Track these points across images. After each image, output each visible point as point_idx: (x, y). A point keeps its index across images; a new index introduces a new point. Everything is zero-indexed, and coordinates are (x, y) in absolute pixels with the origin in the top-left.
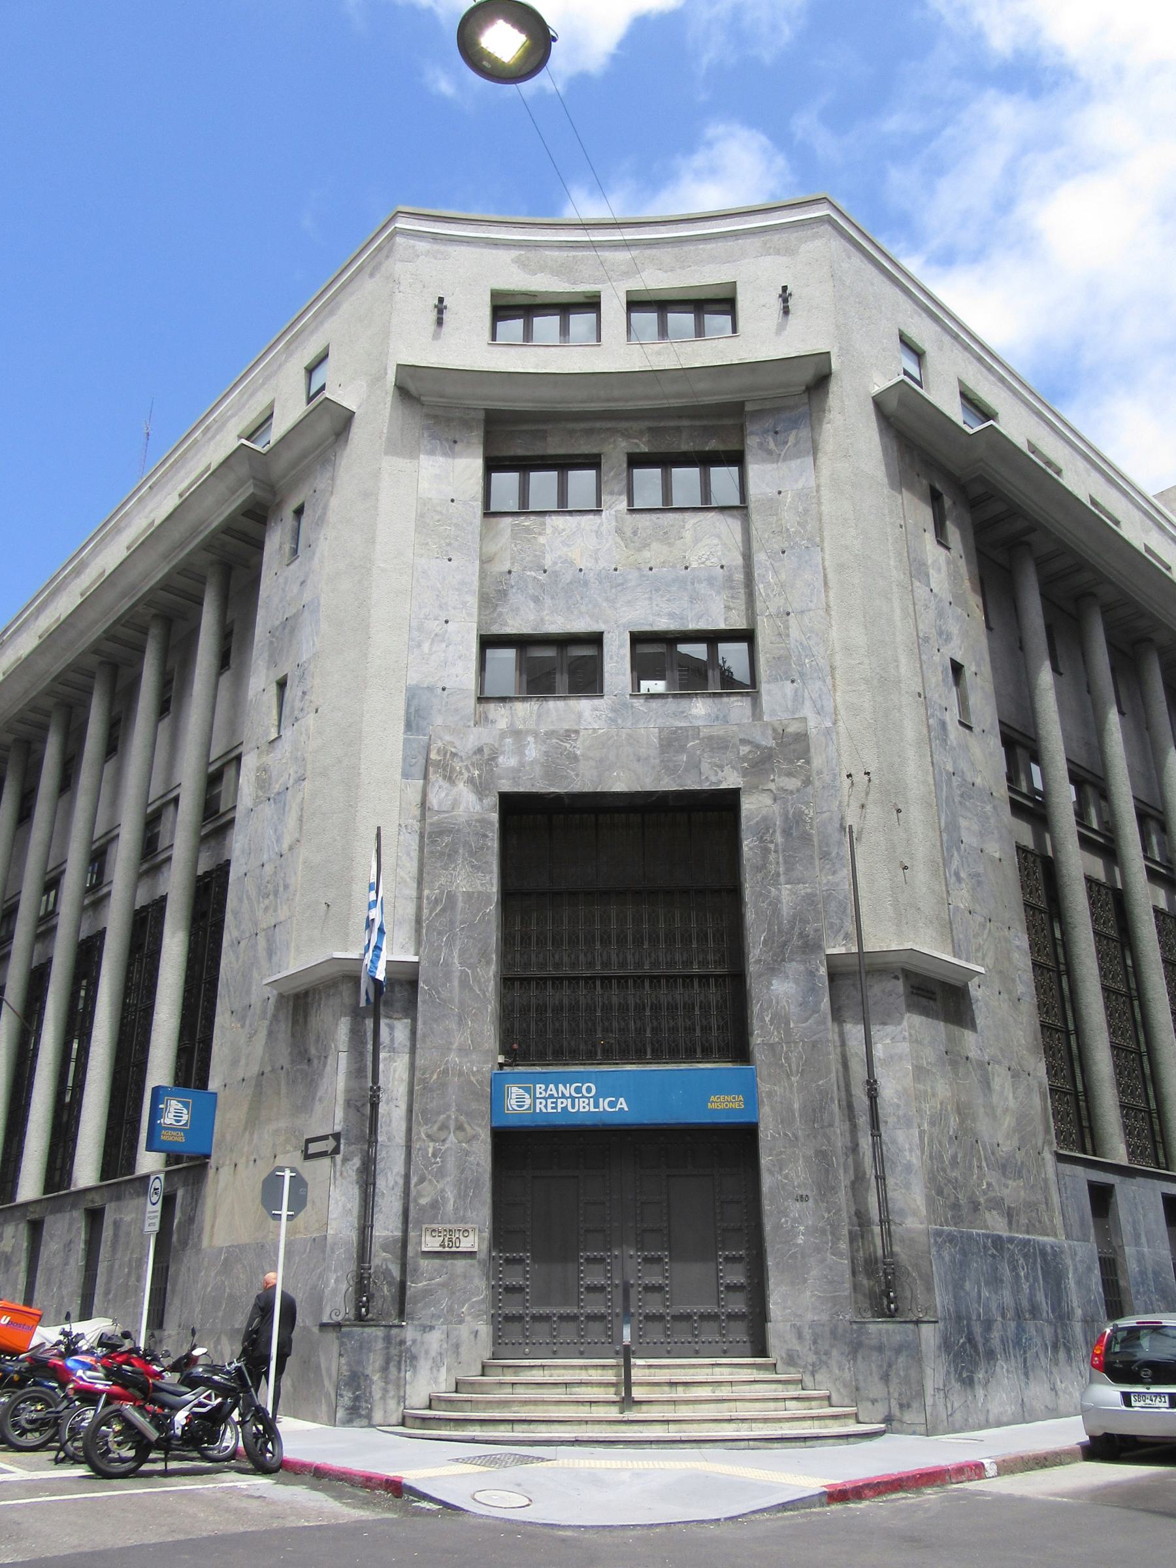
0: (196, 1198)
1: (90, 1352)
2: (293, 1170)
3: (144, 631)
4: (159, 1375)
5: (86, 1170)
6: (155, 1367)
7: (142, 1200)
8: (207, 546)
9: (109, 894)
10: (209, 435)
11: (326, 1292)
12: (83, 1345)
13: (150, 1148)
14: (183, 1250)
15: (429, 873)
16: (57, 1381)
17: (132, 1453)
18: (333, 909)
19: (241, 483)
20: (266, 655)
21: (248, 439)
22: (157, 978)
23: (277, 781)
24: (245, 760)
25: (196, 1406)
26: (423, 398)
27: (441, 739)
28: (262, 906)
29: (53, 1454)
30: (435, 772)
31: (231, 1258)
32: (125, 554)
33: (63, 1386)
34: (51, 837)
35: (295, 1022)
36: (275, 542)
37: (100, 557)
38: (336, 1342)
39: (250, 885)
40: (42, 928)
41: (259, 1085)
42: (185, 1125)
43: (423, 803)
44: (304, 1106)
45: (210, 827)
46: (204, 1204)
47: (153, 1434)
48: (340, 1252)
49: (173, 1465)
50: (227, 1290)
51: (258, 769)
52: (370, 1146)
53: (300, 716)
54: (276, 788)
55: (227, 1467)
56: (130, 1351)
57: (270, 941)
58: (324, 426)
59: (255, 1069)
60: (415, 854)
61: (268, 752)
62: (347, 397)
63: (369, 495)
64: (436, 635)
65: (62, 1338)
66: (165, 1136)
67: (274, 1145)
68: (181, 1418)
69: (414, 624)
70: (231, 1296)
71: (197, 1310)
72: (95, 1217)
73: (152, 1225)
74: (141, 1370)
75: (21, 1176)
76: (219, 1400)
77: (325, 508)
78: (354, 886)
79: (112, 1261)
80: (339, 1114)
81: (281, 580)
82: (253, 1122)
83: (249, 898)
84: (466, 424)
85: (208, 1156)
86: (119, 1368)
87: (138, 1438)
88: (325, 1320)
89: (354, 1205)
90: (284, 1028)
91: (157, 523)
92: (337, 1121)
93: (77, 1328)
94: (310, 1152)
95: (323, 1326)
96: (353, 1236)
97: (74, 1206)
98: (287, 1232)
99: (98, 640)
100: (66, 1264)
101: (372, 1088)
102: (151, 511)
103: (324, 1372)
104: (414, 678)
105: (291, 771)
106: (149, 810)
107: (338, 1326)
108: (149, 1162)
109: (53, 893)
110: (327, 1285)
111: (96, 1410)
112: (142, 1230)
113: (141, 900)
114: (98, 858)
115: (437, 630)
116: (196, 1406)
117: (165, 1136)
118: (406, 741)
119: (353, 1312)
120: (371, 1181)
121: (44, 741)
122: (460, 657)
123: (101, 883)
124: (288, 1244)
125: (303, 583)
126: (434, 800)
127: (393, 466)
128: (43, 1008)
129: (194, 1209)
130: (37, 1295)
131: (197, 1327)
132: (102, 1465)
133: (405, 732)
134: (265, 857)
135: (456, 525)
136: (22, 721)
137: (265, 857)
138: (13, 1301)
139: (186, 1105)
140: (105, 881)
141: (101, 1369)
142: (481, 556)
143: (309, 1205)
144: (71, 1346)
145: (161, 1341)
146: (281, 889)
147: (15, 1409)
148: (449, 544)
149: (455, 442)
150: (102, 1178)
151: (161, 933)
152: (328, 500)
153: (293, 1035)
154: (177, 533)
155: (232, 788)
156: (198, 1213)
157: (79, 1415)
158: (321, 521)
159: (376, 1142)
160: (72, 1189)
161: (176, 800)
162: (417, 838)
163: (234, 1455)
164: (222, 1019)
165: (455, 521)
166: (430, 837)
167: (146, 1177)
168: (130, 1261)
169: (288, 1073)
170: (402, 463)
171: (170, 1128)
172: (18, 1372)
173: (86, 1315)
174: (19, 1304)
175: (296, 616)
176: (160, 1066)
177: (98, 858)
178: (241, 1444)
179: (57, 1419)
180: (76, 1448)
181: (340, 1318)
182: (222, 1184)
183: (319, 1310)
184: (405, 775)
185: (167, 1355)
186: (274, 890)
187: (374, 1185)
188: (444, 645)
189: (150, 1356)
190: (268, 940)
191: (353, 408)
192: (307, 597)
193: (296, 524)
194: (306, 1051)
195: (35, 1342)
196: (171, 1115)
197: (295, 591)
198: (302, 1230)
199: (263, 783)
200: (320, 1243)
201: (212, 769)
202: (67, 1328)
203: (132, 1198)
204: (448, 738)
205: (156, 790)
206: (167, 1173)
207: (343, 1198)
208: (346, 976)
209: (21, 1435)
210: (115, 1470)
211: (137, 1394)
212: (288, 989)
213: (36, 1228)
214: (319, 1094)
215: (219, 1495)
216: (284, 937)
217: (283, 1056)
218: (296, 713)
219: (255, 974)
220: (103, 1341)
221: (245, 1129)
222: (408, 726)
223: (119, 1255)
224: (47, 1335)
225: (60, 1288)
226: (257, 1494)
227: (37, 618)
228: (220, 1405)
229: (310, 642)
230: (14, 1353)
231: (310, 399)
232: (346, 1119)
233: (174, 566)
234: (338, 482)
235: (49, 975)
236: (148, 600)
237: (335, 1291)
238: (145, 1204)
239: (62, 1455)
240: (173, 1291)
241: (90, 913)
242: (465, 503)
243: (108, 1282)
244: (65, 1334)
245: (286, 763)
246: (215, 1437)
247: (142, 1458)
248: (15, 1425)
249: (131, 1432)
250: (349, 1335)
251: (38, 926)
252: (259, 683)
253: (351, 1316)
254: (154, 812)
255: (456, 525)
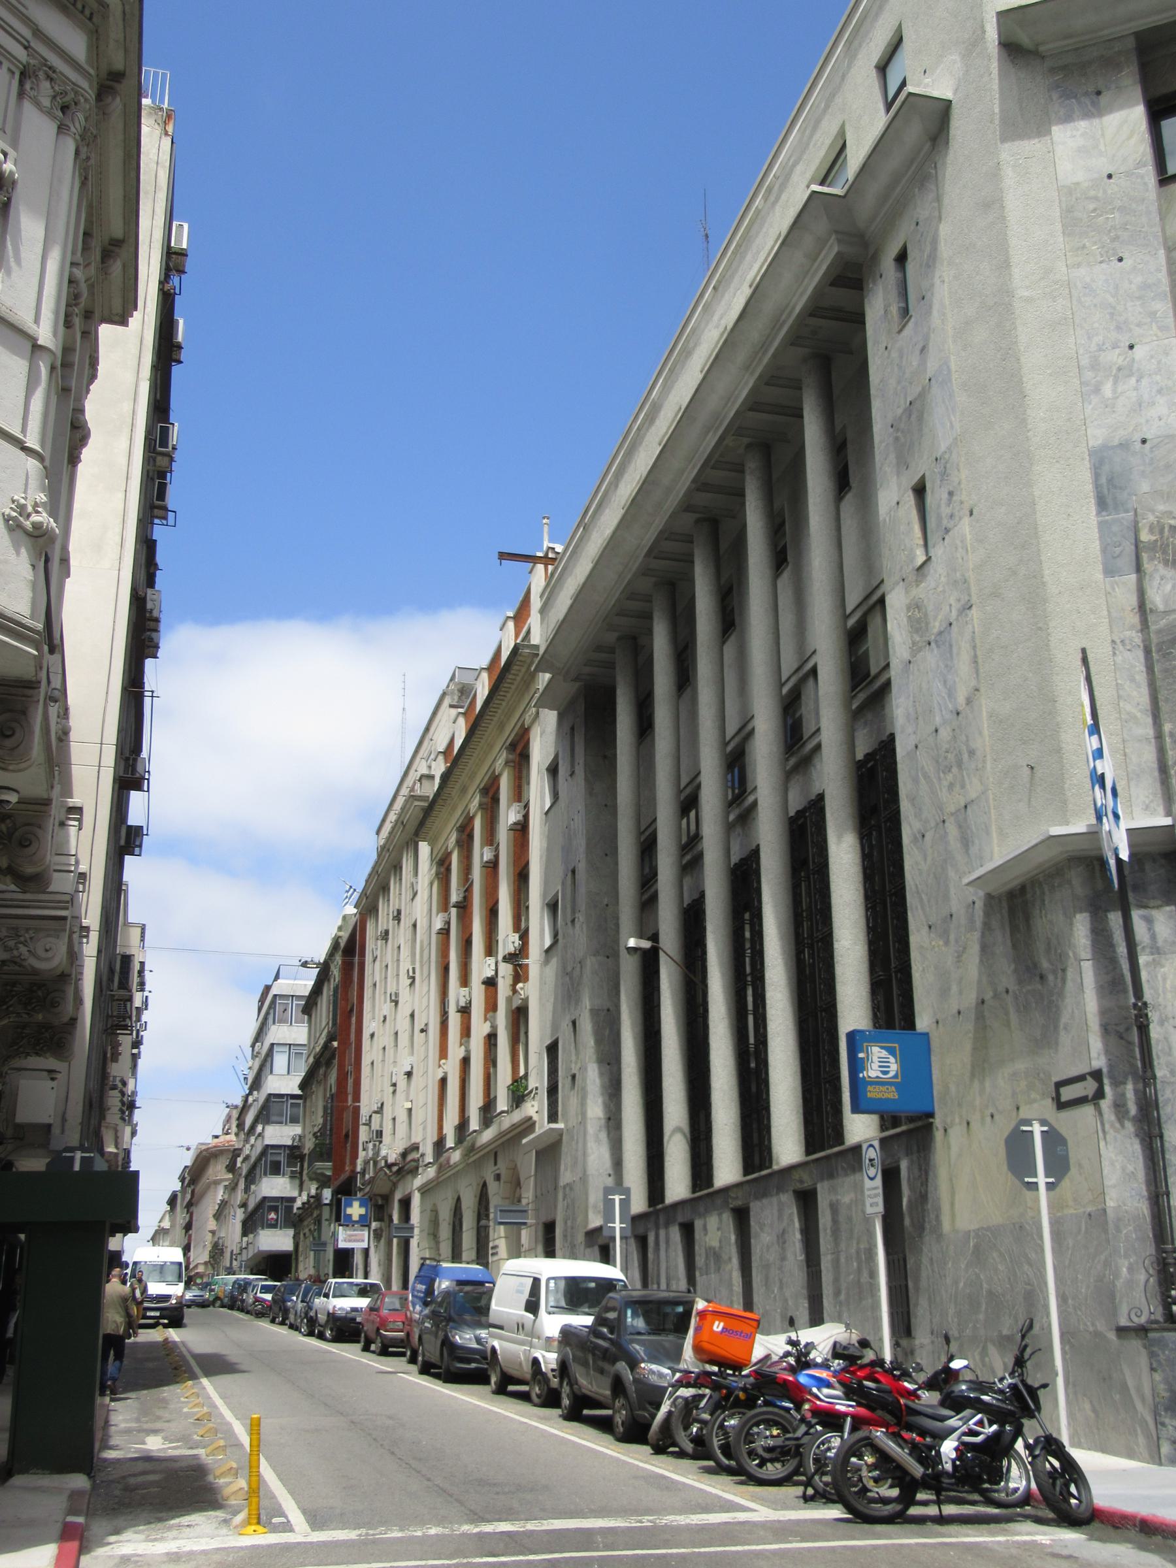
0: (924, 1169)
1: (825, 1365)
2: (1043, 1122)
3: (740, 469)
4: (913, 1394)
5: (787, 1145)
6: (906, 1384)
7: (857, 1176)
8: (795, 339)
9: (755, 803)
10: (772, 198)
11: (1119, 1284)
12: (817, 1356)
13: (856, 1109)
14: (920, 1236)
15: (1167, 700)
16: (792, 1402)
17: (895, 1492)
18: (1039, 772)
19: (822, 243)
20: (892, 457)
21: (822, 183)
22: (829, 897)
23: (935, 618)
24: (889, 600)
25: (965, 1434)
26: (1042, 49)
27: (1153, 511)
28: (945, 783)
29: (799, 1490)
30: (1152, 559)
31: (982, 1244)
32: (701, 376)
33: (798, 1408)
34: (678, 746)
35: (1014, 929)
36: (878, 306)
37: (673, 392)
38: (1144, 1352)
39: (925, 760)
40: (688, 857)
41: (980, 1017)
42: (896, 1076)
43: (1142, 607)
44: (1046, 1036)
45: (862, 697)
46: (936, 1176)
47: (917, 1470)
48: (1128, 1230)
49: (950, 1510)
50: (985, 1286)
51: (909, 608)
52: (1146, 1085)
53: (949, 526)
54: (936, 626)
55: (1019, 1515)
56: (873, 1364)
57: (963, 827)
58: (914, 132)
59: (971, 998)
60: (1142, 677)
61: (918, 583)
62: (937, 84)
63: (992, 204)
64: (1119, 369)
65: (789, 1348)
66: (873, 1093)
67: (1014, 1094)
68: (948, 1448)
69: (1085, 362)
70: (990, 1293)
71: (951, 1311)
72: (807, 1200)
73: (875, 1204)
74: (888, 1387)
75: (715, 1156)
76: (995, 1427)
77: (935, 242)
78: (1063, 736)
79: (836, 1253)
80: (1096, 1044)
81: (895, 355)
82: (981, 1065)
83: (926, 776)
84: (1110, 64)
85: (931, 1115)
86: (860, 1385)
87: (898, 1474)
88: (1123, 1322)
89: (1137, 1165)
90: (1001, 942)
91: (729, 328)
92: (1094, 1054)
93: (806, 1335)
94: (1064, 1099)
95: (1121, 1331)
96: (1143, 1207)
97: (780, 1189)
98: (1051, 1206)
99: (689, 493)
100: (783, 1258)
101: (1135, 1005)
102: (721, 318)
103: (1133, 1392)
104: (1097, 435)
105: (952, 601)
106: (785, 690)
107: (1142, 1331)
108: (860, 1128)
109: (693, 814)
110: (1117, 1275)
111: (842, 1437)
112: (863, 1212)
113: (796, 803)
114: (736, 761)
115: (1120, 361)
116: (965, 1434)
117: (873, 1093)
118: (1101, 525)
119: (1160, 1310)
120: (1157, 1131)
121: (650, 632)
122: (1159, 391)
123: (745, 791)
124: (1055, 1223)
125: (923, 349)
126: (1156, 598)
127: (1011, 153)
128: (704, 953)
129: (925, 1183)
130: (757, 1298)
131: (954, 1333)
132: (860, 1506)
133: (1098, 514)
134: (938, 719)
135: (1122, 209)
136: (621, 613)
137: (938, 719)
138: (731, 1306)
139: (891, 1051)
140: (749, 788)
141: (837, 1385)
142: (1165, 240)
143: (1073, 1170)
144: (803, 1361)
145: (912, 1352)
146: (966, 756)
147: (748, 1433)
148: (1117, 238)
149: (1099, 93)
150: (808, 1152)
151: (825, 841)
152: (937, 230)
153: (1014, 946)
154: (755, 333)
155: (881, 641)
156: (931, 1189)
157: (823, 1443)
158: (931, 262)
159: (1154, 1077)
160: (775, 1167)
161: (814, 671)
162: (1141, 654)
163: (1027, 1499)
164: (918, 938)
165: (1118, 203)
166: (1159, 651)
167: (857, 1149)
168: (858, 1252)
169: (1016, 998)
170: (1031, 146)
171: (877, 1082)
172: (744, 1389)
173: (816, 1319)
174: (738, 1309)
175: (922, 395)
176: (853, 1007)
177: (736, 761)
178: (1033, 1485)
179: (798, 1446)
180: (826, 1484)
181: (1143, 1320)
182: (954, 1150)
183: (1114, 1311)
184: (1109, 571)
185: (919, 1369)
186: (956, 760)
187: (1161, 1136)
188: (1133, 380)
189: (900, 1371)
190: (960, 827)
191: (948, 94)
192: (932, 366)
193: (900, 275)
194: (1035, 965)
195: (758, 1353)
196: (875, 1066)
197: (915, 363)
198: (1071, 1203)
199: (918, 624)
200: (1098, 1219)
201: (851, 622)
202: (793, 1336)
203: (846, 1175)
204: (1161, 507)
205: (789, 664)
206: (883, 1141)
207: (1120, 1158)
208: (1086, 859)
209: (760, 1465)
210: (876, 1513)
211: (888, 1417)
212: (998, 886)
213: (742, 1217)
214: (1064, 1019)
215: (1014, 1551)
216: (981, 822)
217: (1007, 978)
218: (945, 522)
219: (951, 873)
220: (838, 1351)
221: (973, 1075)
222: (1102, 504)
223: (843, 1246)
224: (769, 1346)
225: (781, 1288)
226: (1065, 1552)
227: (617, 486)
228: (996, 1436)
229: (946, 425)
230: (737, 1367)
231: (889, 106)
232: (1107, 1052)
233: (760, 376)
234: (946, 201)
235: (704, 912)
236: (736, 428)
237: (1130, 1284)
238: (863, 1181)
239: (810, 1491)
240: (917, 1289)
241: (739, 830)
242: (1129, 174)
243: (836, 1280)
244: (791, 1343)
245: (944, 591)
246: (998, 1475)
247: (907, 1499)
248: (752, 1453)
249: (887, 1466)
250: (1161, 1343)
251: (683, 856)
252: (891, 496)
253: (1159, 1316)
254: (791, 691)
255: (1122, 209)
